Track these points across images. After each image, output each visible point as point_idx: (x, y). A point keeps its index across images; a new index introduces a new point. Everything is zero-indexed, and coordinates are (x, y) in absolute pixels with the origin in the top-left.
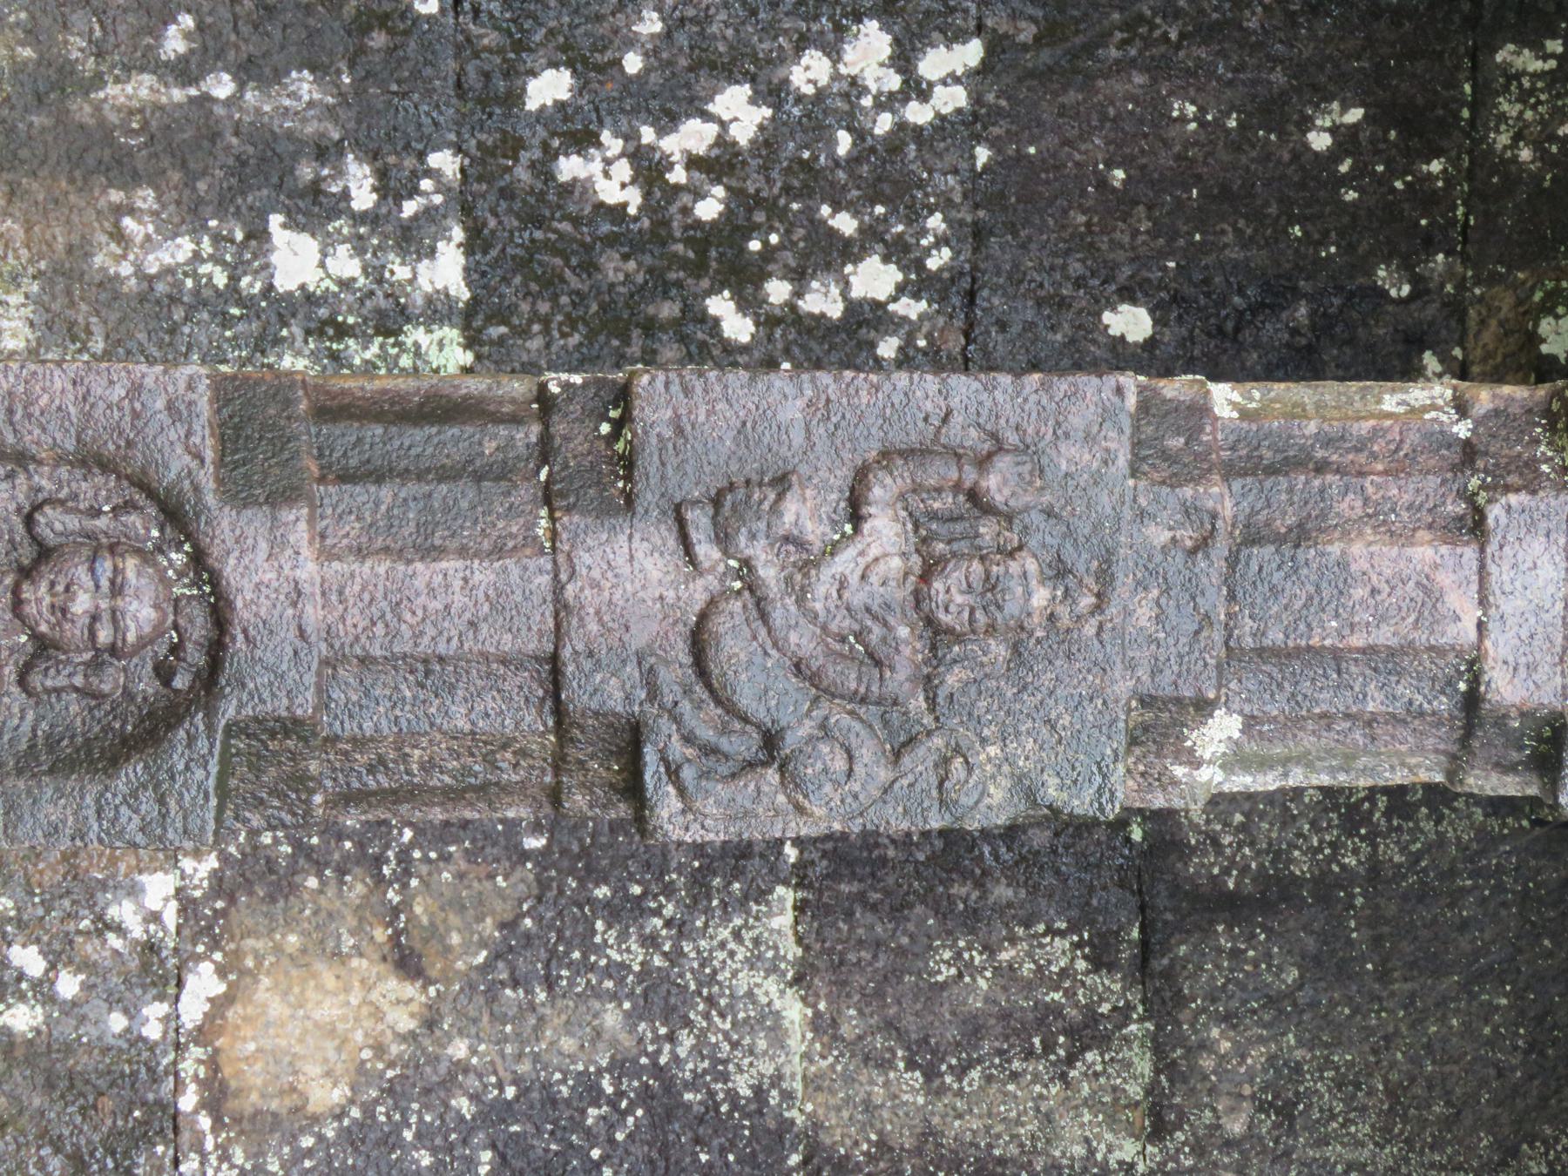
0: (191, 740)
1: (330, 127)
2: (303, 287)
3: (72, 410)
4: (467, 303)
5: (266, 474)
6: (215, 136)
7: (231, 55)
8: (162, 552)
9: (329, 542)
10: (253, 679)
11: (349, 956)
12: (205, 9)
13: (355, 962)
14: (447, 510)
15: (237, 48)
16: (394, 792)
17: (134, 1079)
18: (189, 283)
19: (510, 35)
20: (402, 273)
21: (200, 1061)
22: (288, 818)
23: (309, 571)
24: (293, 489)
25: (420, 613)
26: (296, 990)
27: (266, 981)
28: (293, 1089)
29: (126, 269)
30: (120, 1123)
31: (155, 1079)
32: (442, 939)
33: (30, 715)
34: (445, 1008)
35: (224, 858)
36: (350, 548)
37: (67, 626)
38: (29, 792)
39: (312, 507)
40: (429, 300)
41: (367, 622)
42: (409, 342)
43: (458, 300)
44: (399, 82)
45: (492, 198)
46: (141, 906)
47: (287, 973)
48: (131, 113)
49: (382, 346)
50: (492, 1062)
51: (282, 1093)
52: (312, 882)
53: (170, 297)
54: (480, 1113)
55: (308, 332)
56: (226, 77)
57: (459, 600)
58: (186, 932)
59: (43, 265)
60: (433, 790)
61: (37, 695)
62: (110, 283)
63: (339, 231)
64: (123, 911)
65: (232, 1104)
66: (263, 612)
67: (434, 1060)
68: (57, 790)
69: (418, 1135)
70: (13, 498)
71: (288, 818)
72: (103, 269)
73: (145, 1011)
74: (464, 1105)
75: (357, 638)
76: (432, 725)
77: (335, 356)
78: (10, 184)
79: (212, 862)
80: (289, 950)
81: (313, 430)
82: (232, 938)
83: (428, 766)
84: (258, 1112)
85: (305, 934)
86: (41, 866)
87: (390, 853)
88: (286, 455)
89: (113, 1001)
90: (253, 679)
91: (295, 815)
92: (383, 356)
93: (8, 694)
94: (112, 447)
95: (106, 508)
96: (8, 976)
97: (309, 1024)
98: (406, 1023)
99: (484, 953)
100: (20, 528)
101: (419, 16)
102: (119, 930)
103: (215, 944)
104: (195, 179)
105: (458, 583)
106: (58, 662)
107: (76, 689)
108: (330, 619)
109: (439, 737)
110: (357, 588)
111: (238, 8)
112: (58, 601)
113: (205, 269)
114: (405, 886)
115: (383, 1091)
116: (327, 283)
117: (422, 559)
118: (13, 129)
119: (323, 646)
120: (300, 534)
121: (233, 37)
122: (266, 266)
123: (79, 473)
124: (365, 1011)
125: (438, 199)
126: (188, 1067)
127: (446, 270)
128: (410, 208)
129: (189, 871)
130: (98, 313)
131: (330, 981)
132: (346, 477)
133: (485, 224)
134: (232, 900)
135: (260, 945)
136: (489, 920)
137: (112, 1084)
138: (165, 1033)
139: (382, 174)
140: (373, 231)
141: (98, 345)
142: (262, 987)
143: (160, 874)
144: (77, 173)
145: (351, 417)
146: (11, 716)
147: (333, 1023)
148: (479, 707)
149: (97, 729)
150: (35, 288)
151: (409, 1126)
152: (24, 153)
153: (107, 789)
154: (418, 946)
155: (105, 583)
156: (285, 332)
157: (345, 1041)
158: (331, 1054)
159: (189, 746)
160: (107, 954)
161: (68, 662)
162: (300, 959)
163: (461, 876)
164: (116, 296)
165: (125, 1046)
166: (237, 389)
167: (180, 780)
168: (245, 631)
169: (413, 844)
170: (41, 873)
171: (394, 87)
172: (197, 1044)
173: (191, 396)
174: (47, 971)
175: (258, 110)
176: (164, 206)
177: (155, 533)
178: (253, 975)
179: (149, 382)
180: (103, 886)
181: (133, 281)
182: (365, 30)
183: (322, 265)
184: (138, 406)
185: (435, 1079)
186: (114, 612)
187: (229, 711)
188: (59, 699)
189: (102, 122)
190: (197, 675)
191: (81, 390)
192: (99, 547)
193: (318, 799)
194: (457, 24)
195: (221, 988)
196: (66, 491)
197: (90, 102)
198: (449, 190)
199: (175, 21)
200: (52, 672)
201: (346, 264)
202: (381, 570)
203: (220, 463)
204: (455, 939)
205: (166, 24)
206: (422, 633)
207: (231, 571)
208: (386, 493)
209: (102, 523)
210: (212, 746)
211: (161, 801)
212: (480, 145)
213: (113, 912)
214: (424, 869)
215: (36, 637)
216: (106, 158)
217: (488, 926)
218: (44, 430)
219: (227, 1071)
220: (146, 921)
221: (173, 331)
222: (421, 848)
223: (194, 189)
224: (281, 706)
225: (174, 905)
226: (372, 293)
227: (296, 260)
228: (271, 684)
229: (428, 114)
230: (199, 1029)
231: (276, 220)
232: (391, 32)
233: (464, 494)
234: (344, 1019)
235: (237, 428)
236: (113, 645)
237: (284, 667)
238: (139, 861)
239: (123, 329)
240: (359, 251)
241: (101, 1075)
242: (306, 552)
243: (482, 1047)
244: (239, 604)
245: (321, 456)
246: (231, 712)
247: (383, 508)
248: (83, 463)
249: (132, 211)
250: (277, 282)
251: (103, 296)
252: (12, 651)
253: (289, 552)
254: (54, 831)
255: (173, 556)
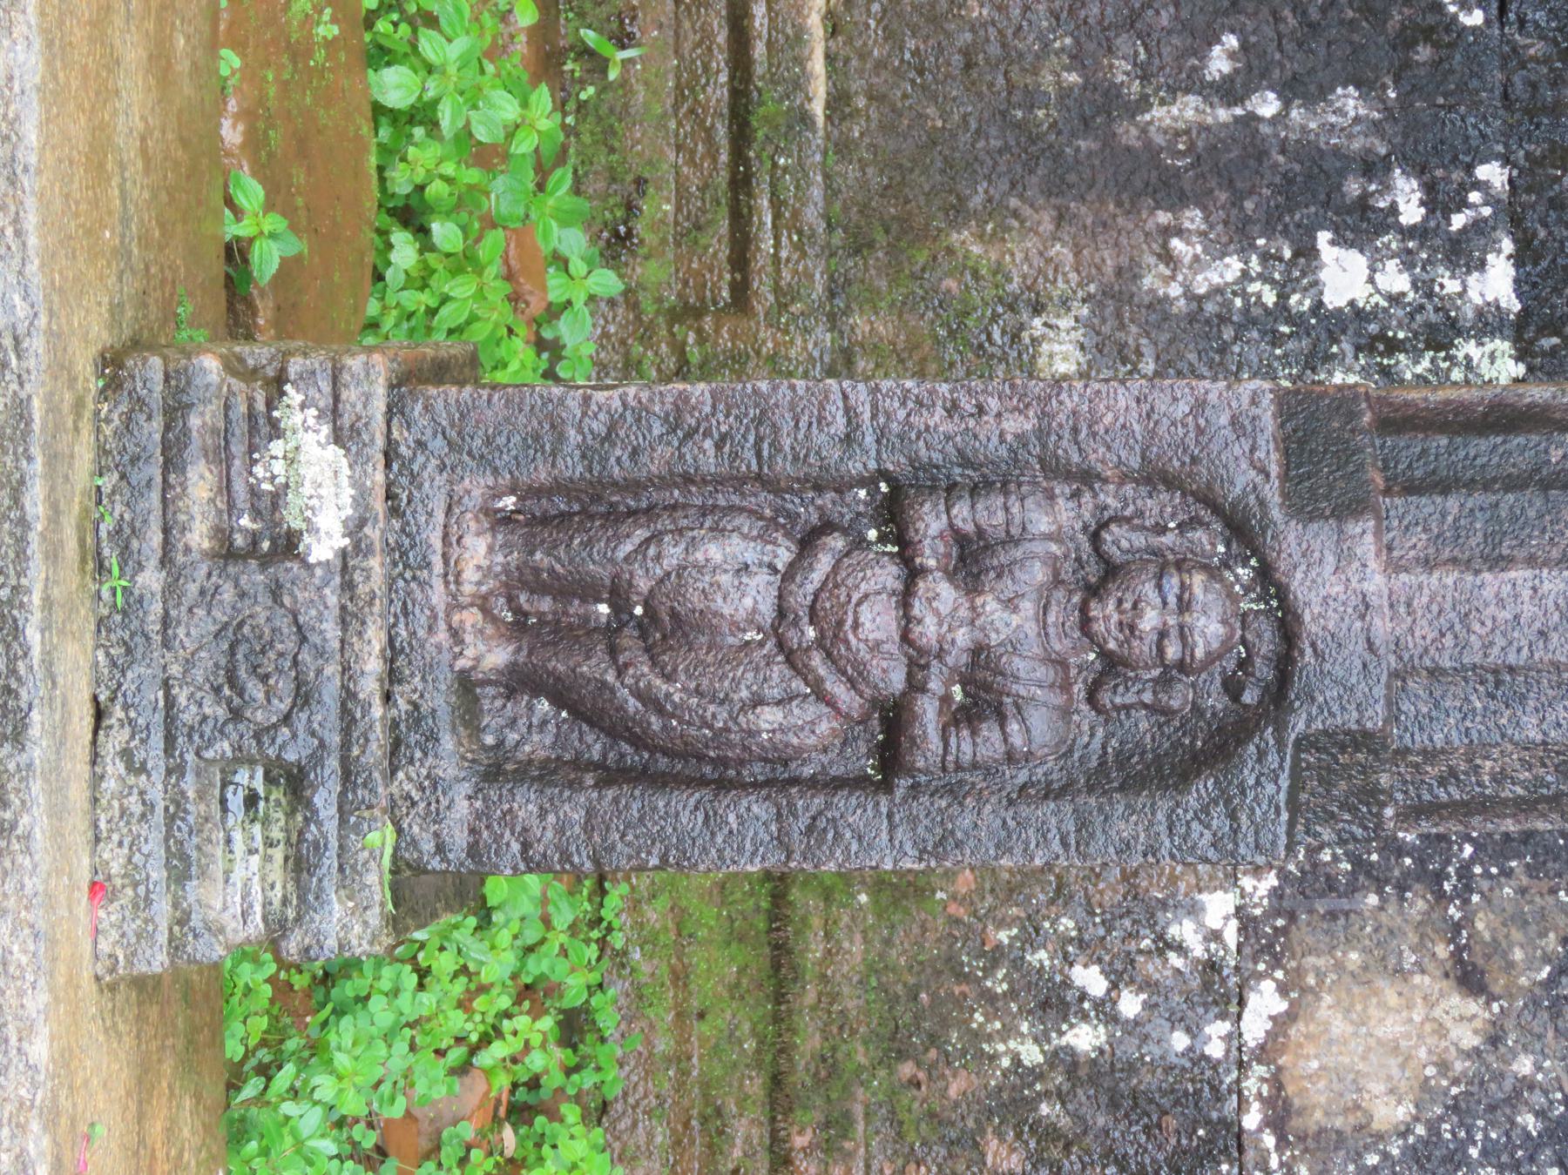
0: (1261, 755)
1: (1377, 142)
2: (1352, 303)
3: (1136, 427)
4: (1518, 315)
5: (1331, 488)
6: (1262, 154)
7: (1276, 74)
8: (1228, 567)
9: (1396, 554)
10: (1322, 692)
11: (1411, 973)
12: (1250, 28)
13: (1417, 979)
14: (1514, 519)
15: (1281, 64)
16: (1464, 804)
17: (1198, 1094)
18: (1238, 302)
19: (1557, 44)
20: (1452, 286)
21: (1263, 1080)
22: (1359, 832)
23: (1376, 583)
24: (1358, 502)
25: (1489, 623)
26: (1359, 1007)
27: (1328, 999)
28: (1358, 1107)
29: (1175, 290)
30: (1184, 1142)
31: (1218, 1097)
32: (1505, 954)
33: (1100, 732)
34: (1510, 1024)
35: (1283, 875)
36: (1417, 559)
37: (1136, 643)
38: (1100, 809)
39: (1379, 519)
40: (1480, 313)
41: (1436, 634)
42: (1460, 355)
43: (1509, 312)
44: (1445, 95)
45: (1541, 208)
46: (1200, 924)
47: (1349, 991)
48: (1177, 134)
49: (1433, 361)
50: (1558, 1079)
51: (1346, 1111)
52: (1373, 899)
53: (1218, 316)
54: (1546, 1129)
55: (1358, 349)
56: (1271, 96)
57: (1528, 610)
58: (1247, 950)
59: (1092, 288)
60: (1504, 802)
61: (1107, 712)
62: (1159, 304)
63: (1387, 246)
64: (1184, 931)
65: (1295, 1123)
66: (1331, 625)
67: (1499, 1076)
68: (1128, 806)
69: (1484, 1153)
70: (1080, 516)
71: (1359, 832)
72: (1152, 291)
73: (1208, 1030)
74: (1529, 1122)
75: (1426, 650)
76: (1503, 736)
77: (1385, 372)
78: (1057, 208)
79: (1272, 880)
80: (1351, 967)
81: (1378, 442)
82: (1293, 957)
83: (1499, 778)
84: (1322, 1131)
85: (1366, 951)
86: (1101, 886)
87: (1451, 869)
88: (1351, 468)
89: (1175, 1020)
90: (1322, 692)
91: (1365, 828)
92: (1435, 370)
93: (1078, 712)
94: (1176, 464)
95: (1172, 525)
96: (1070, 996)
97: (1372, 1042)
98: (1470, 1040)
99: (1548, 969)
100: (1086, 547)
101: (1465, 28)
102: (1180, 949)
103: (1277, 962)
104: (1242, 199)
105: (1527, 593)
106: (1127, 679)
107: (1146, 706)
108: (1398, 631)
109: (1510, 747)
110: (1425, 600)
111: (1282, 27)
112: (1126, 618)
113: (1254, 287)
114: (1466, 901)
115: (1447, 1108)
116: (1377, 298)
117: (1490, 569)
118: (1061, 153)
119: (1392, 658)
120: (1367, 546)
121: (1277, 56)
122: (1316, 283)
123: (1144, 490)
124: (1428, 1027)
125: (1487, 211)
126: (1251, 1085)
127: (1496, 284)
128: (1458, 221)
129: (1249, 889)
130: (1148, 335)
131: (1392, 999)
132: (1412, 488)
133: (1535, 235)
134: (1292, 917)
135: (1321, 962)
136: (1552, 935)
137: (1177, 1103)
138: (1228, 1051)
139: (1430, 188)
140: (1422, 246)
141: (1149, 366)
142: (1323, 1005)
143: (1220, 893)
144: (1124, 196)
145: (1415, 428)
146: (1081, 733)
147: (1396, 1040)
148: (1550, 717)
149: (1167, 745)
150: (1085, 311)
151: (1474, 1143)
152: (1072, 178)
153: (1178, 805)
154: (1480, 962)
155: (1172, 600)
156: (1335, 349)
157: (1408, 1058)
158: (1395, 1072)
159: (1259, 760)
160: (1168, 973)
161: (1137, 678)
162: (1361, 978)
163: (1523, 891)
164: (1166, 317)
165: (1188, 1065)
166: (1300, 403)
167: (1251, 795)
168: (1313, 645)
169: (1474, 859)
170: (1101, 893)
171: (1441, 101)
172: (1260, 1062)
173: (1255, 411)
174: (1109, 991)
175: (1304, 129)
176: (1211, 227)
177: (1221, 549)
178: (1315, 993)
179: (1213, 397)
180: (1164, 905)
181: (1182, 302)
182: (1411, 45)
183: (1371, 280)
184: (1202, 422)
185: (1500, 1095)
186: (1181, 627)
187: (1298, 725)
188: (1128, 716)
189: (1148, 144)
190: (1266, 690)
191: (1145, 407)
192: (1164, 564)
193: (1389, 812)
194: (1503, 35)
195: (1283, 1006)
196: (1131, 508)
197: (1136, 125)
198: (1498, 201)
199: (1219, 41)
200: (1121, 689)
201: (1395, 279)
202: (1449, 581)
203: (1285, 477)
204: (1518, 955)
205: (1210, 45)
206: (1492, 644)
207: (1298, 585)
208: (1452, 504)
209: (1168, 539)
210: (1282, 760)
211: (1233, 816)
212: (1528, 155)
213: (1173, 931)
214: (1485, 885)
215: (1104, 654)
216: (1153, 180)
217: (1551, 942)
218: (1109, 448)
219: (1290, 1089)
220: (1206, 939)
221: (1223, 350)
222: (1482, 864)
223: (1242, 208)
224: (1350, 719)
225: (1234, 924)
226: (1422, 307)
227: (1346, 276)
228: (1340, 697)
229: (1475, 126)
230: (1262, 1047)
231: (1323, 237)
232: (1436, 45)
233: (1531, 502)
234: (1408, 1036)
235: (1302, 443)
236: (1182, 660)
237: (1354, 680)
238: (1199, 880)
239: (1173, 351)
240: (1408, 265)
241: (1164, 1094)
242: (1373, 565)
243: (1547, 1064)
244: (1307, 617)
245: (1385, 468)
246: (1301, 726)
247: (1450, 519)
248: (1148, 480)
249: (1179, 232)
250: (1326, 300)
251: (1153, 317)
252: (1080, 669)
253: (1356, 564)
254: (1126, 847)
255: (1240, 571)
